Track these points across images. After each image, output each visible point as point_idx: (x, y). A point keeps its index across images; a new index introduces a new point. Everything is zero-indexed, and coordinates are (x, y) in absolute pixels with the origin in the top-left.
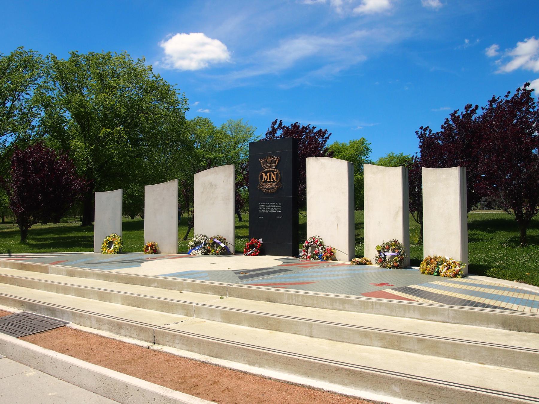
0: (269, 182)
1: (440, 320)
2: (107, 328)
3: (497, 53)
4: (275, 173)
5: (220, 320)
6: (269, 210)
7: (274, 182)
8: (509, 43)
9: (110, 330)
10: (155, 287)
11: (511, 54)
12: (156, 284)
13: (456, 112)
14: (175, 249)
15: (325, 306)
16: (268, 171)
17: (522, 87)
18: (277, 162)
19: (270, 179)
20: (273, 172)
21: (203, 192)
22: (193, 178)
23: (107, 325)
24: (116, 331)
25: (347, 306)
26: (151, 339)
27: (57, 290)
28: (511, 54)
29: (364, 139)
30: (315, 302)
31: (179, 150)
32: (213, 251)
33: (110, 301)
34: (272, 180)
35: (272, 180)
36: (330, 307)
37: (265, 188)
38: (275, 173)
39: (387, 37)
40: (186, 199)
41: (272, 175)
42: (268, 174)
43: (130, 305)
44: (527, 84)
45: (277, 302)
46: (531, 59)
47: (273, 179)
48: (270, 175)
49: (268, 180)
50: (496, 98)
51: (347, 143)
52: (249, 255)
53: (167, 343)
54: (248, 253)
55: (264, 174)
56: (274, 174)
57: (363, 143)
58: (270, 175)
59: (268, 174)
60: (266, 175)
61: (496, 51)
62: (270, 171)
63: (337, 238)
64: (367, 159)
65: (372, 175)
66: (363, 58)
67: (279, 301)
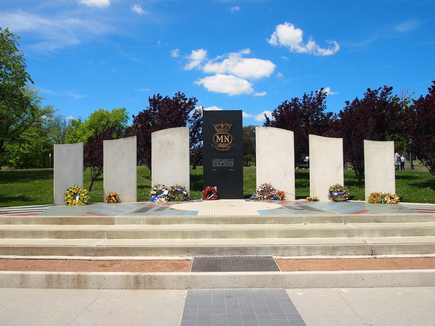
0: (222, 143)
1: (36, 261)
2: (320, 253)
3: (178, 55)
4: (228, 136)
5: (379, 235)
6: (223, 164)
7: (227, 142)
8: (187, 51)
9: (323, 254)
10: (271, 223)
11: (188, 58)
12: (272, 221)
13: (286, 102)
14: (135, 199)
15: (415, 220)
16: (222, 135)
17: (319, 91)
18: (229, 128)
19: (224, 140)
20: (226, 135)
21: (160, 149)
22: (150, 138)
23: (320, 251)
24: (330, 254)
25: (428, 219)
26: (368, 253)
27: (183, 236)
28: (188, 58)
29: (125, 109)
30: (409, 219)
31: (414, 125)
32: (177, 198)
33: (263, 237)
34: (225, 142)
35: (225, 142)
36: (418, 221)
37: (219, 148)
38: (228, 136)
39: (98, 28)
40: (144, 156)
41: (226, 137)
42: (222, 136)
43: (287, 237)
44: (322, 89)
45: (382, 222)
46: (200, 64)
47: (226, 140)
48: (224, 138)
49: (222, 141)
50: (307, 95)
51: (110, 112)
52: (209, 200)
53: (384, 253)
54: (208, 199)
55: (218, 136)
56: (227, 137)
57: (123, 112)
58: (224, 138)
59: (222, 136)
60: (220, 137)
61: (178, 54)
62: (223, 135)
63: (286, 184)
64: (126, 125)
65: (315, 142)
66: (76, 42)
67: (384, 221)
